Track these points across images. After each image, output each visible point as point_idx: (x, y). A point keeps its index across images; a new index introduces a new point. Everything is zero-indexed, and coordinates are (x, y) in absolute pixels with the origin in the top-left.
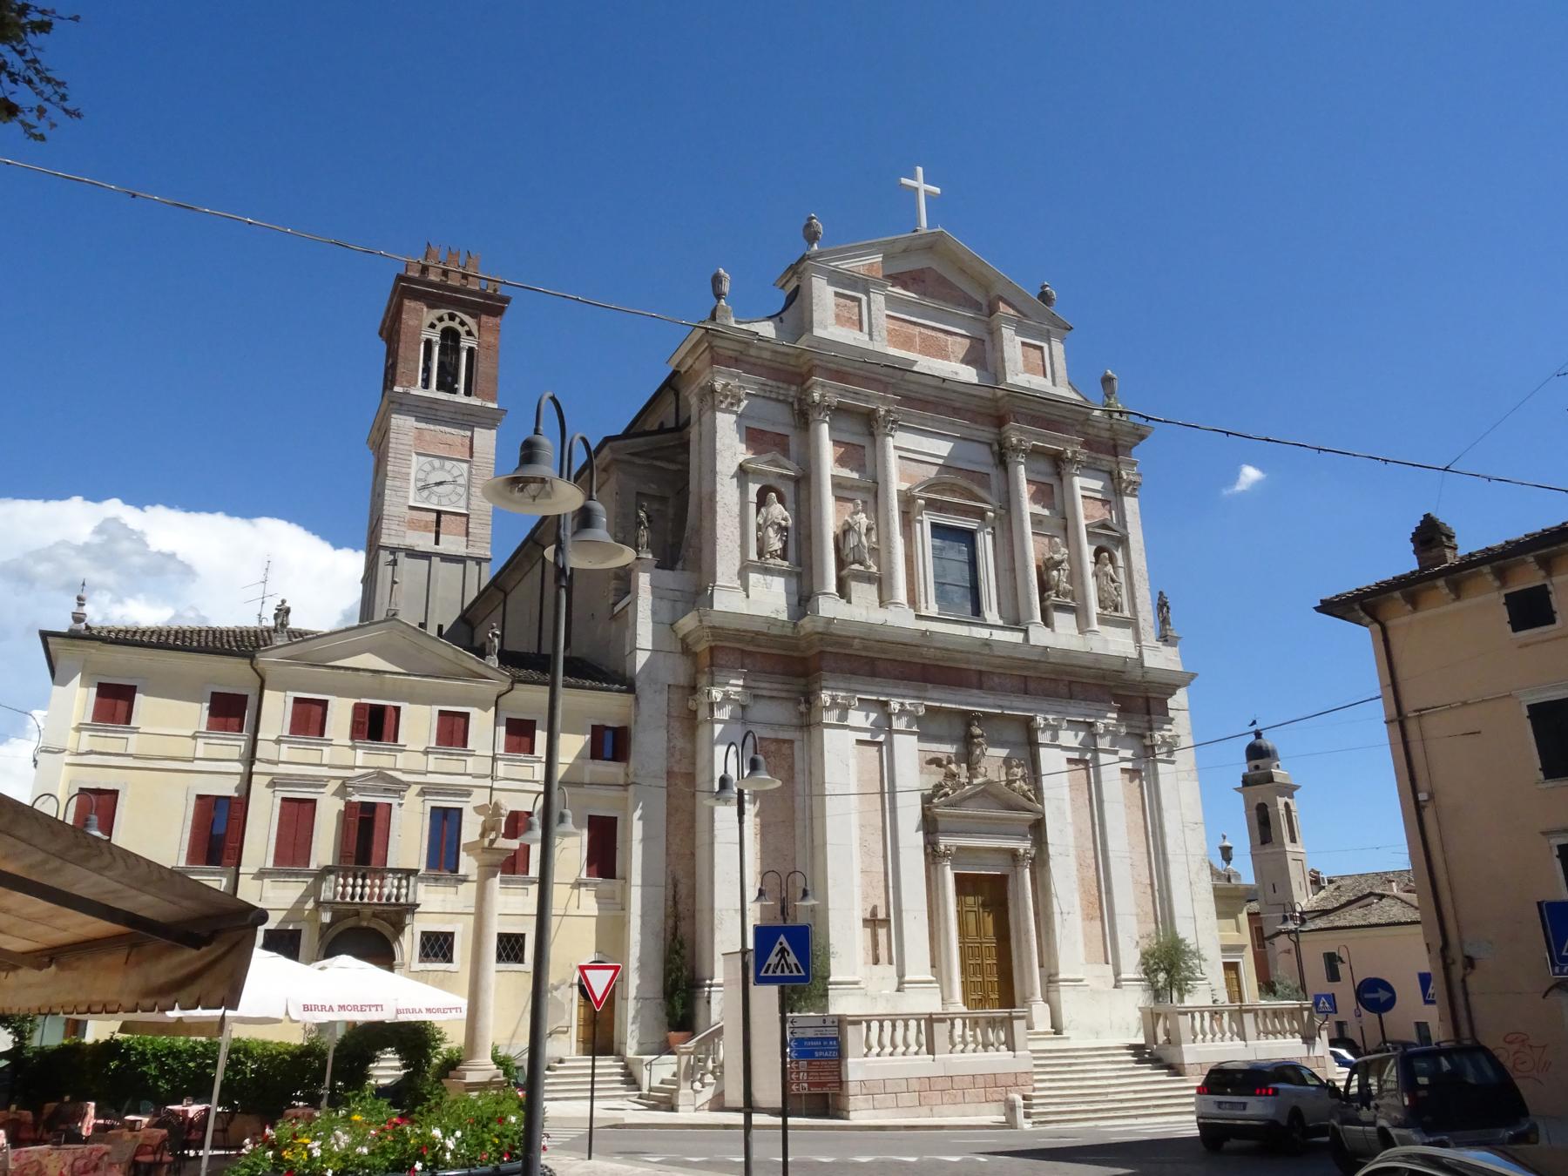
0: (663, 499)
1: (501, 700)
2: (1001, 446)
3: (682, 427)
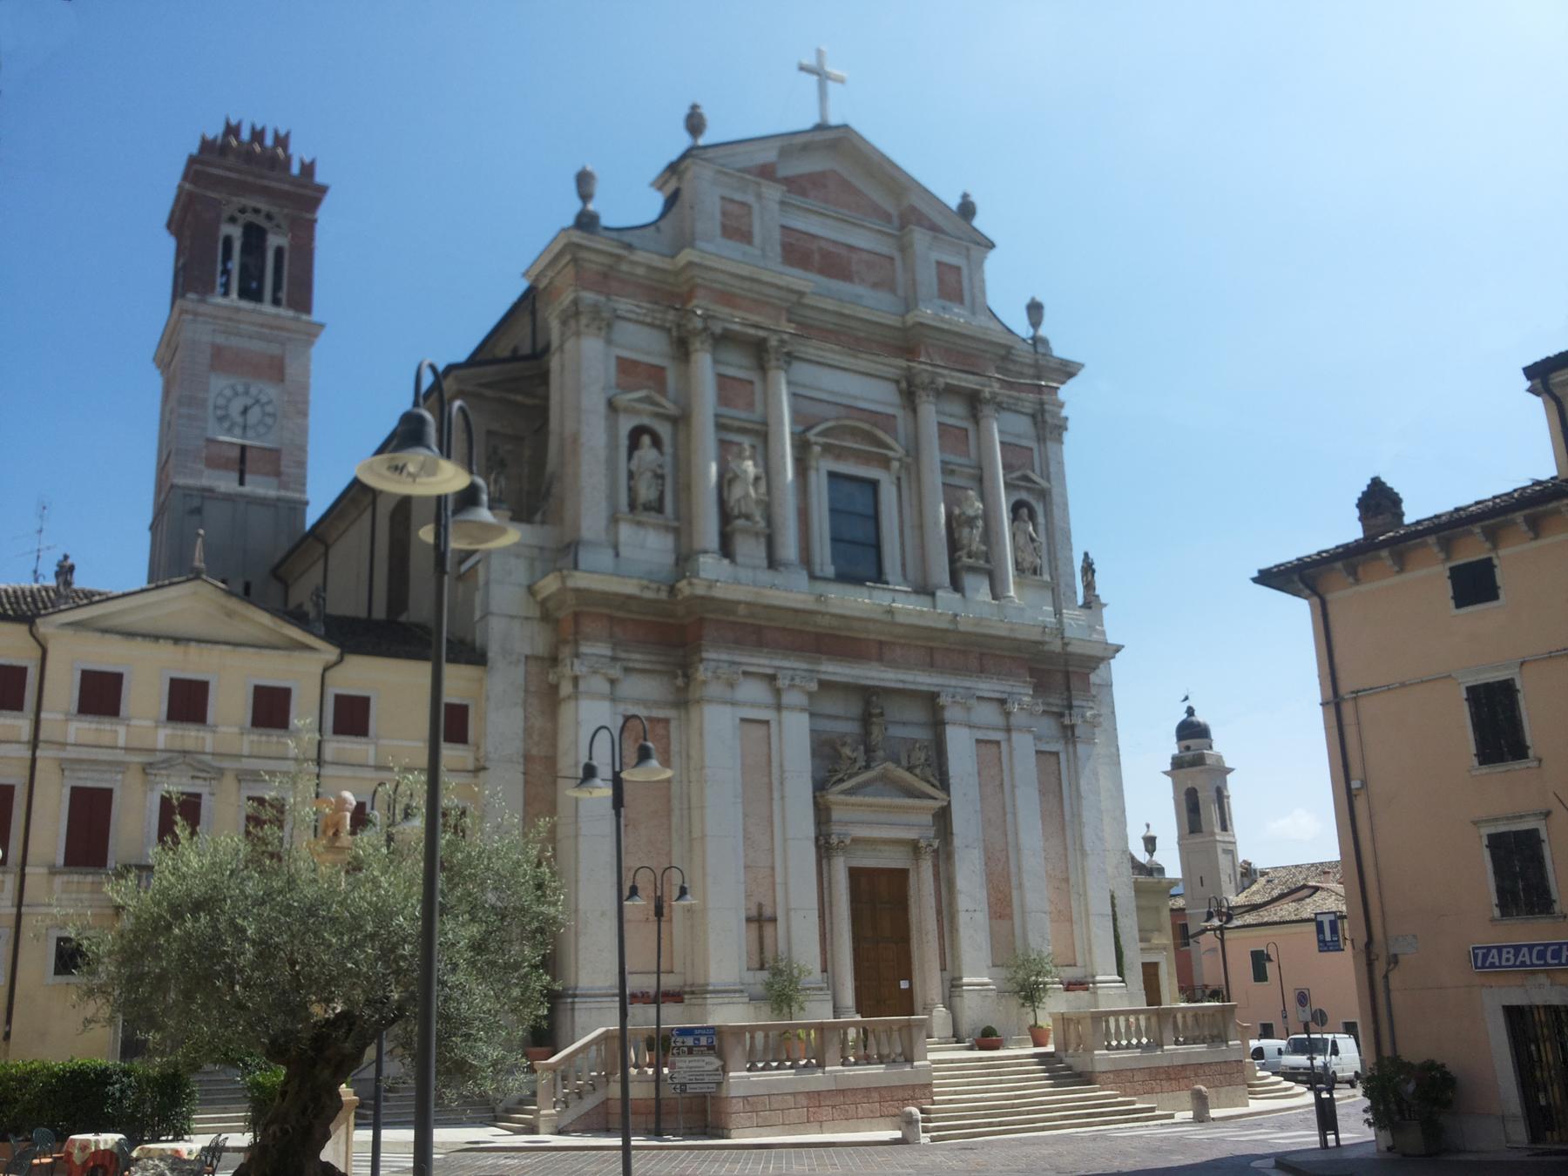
1: (329, 674)
2: (910, 384)
3: (540, 354)
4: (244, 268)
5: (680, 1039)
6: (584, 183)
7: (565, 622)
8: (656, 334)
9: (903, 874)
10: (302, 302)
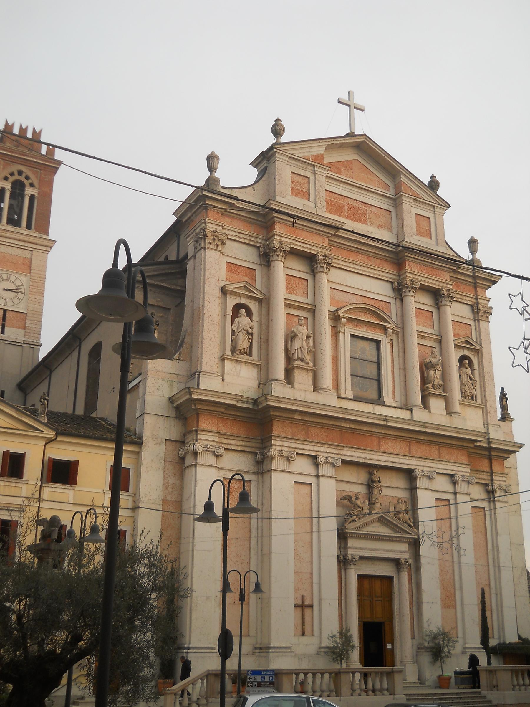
2: (399, 284)
4: (11, 207)
5: (253, 677)
6: (212, 161)
7: (186, 411)
8: (251, 249)
9: (390, 579)
10: (44, 228)
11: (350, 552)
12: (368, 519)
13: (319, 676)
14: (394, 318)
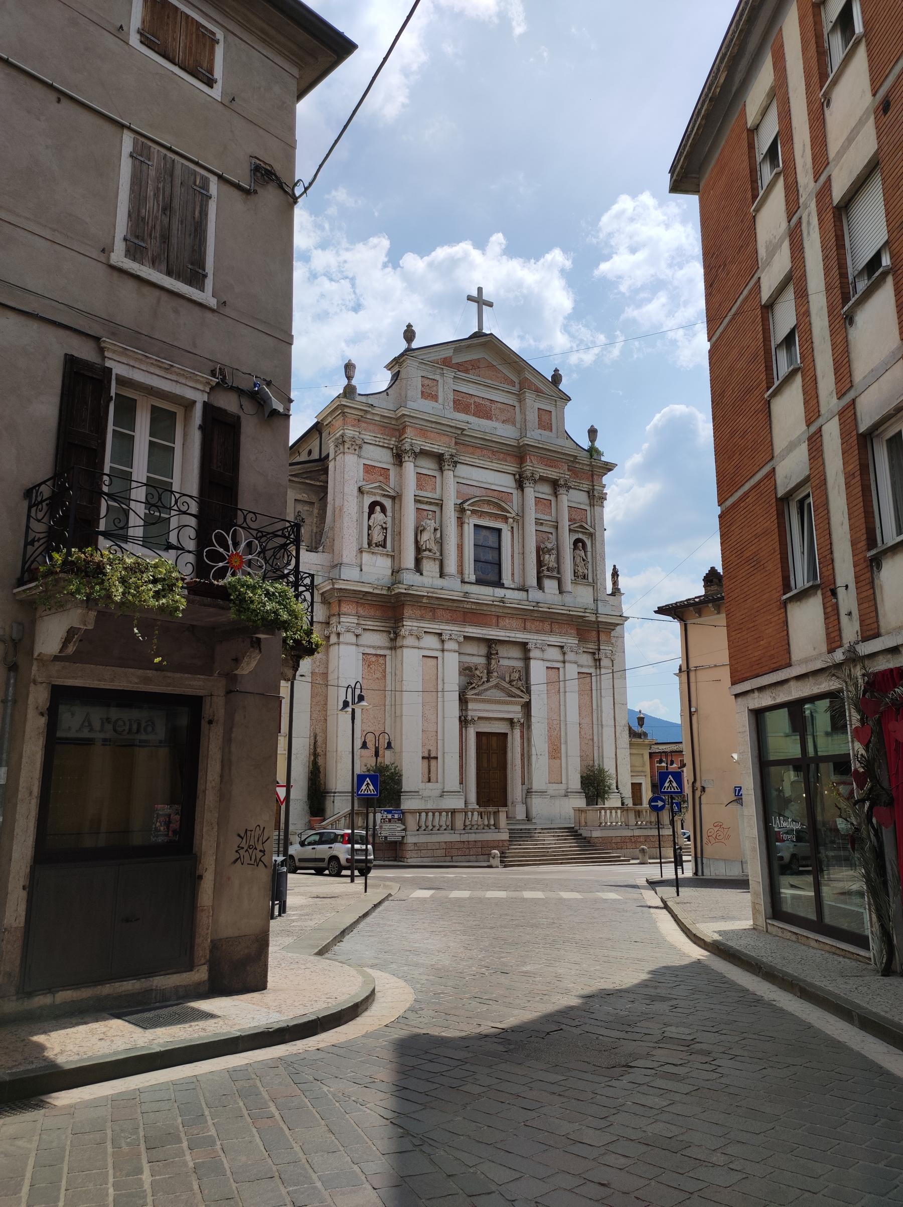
0: (311, 503)
9: (506, 734)
11: (470, 713)
12: (487, 685)
13: (437, 814)
14: (515, 508)
